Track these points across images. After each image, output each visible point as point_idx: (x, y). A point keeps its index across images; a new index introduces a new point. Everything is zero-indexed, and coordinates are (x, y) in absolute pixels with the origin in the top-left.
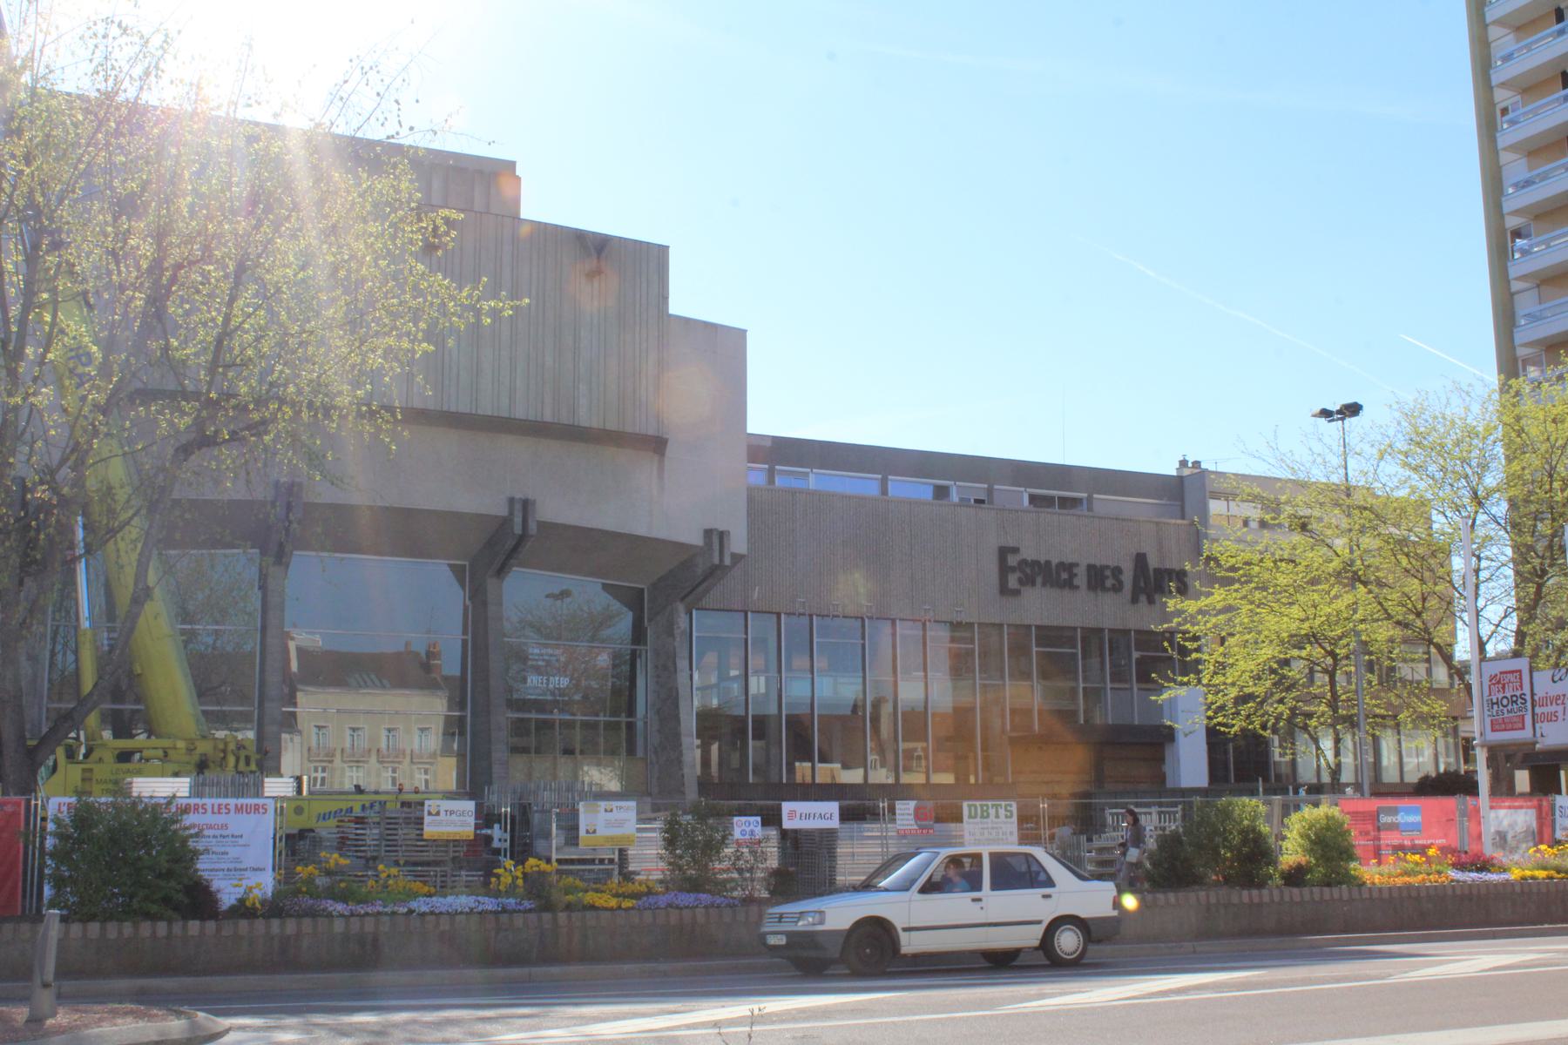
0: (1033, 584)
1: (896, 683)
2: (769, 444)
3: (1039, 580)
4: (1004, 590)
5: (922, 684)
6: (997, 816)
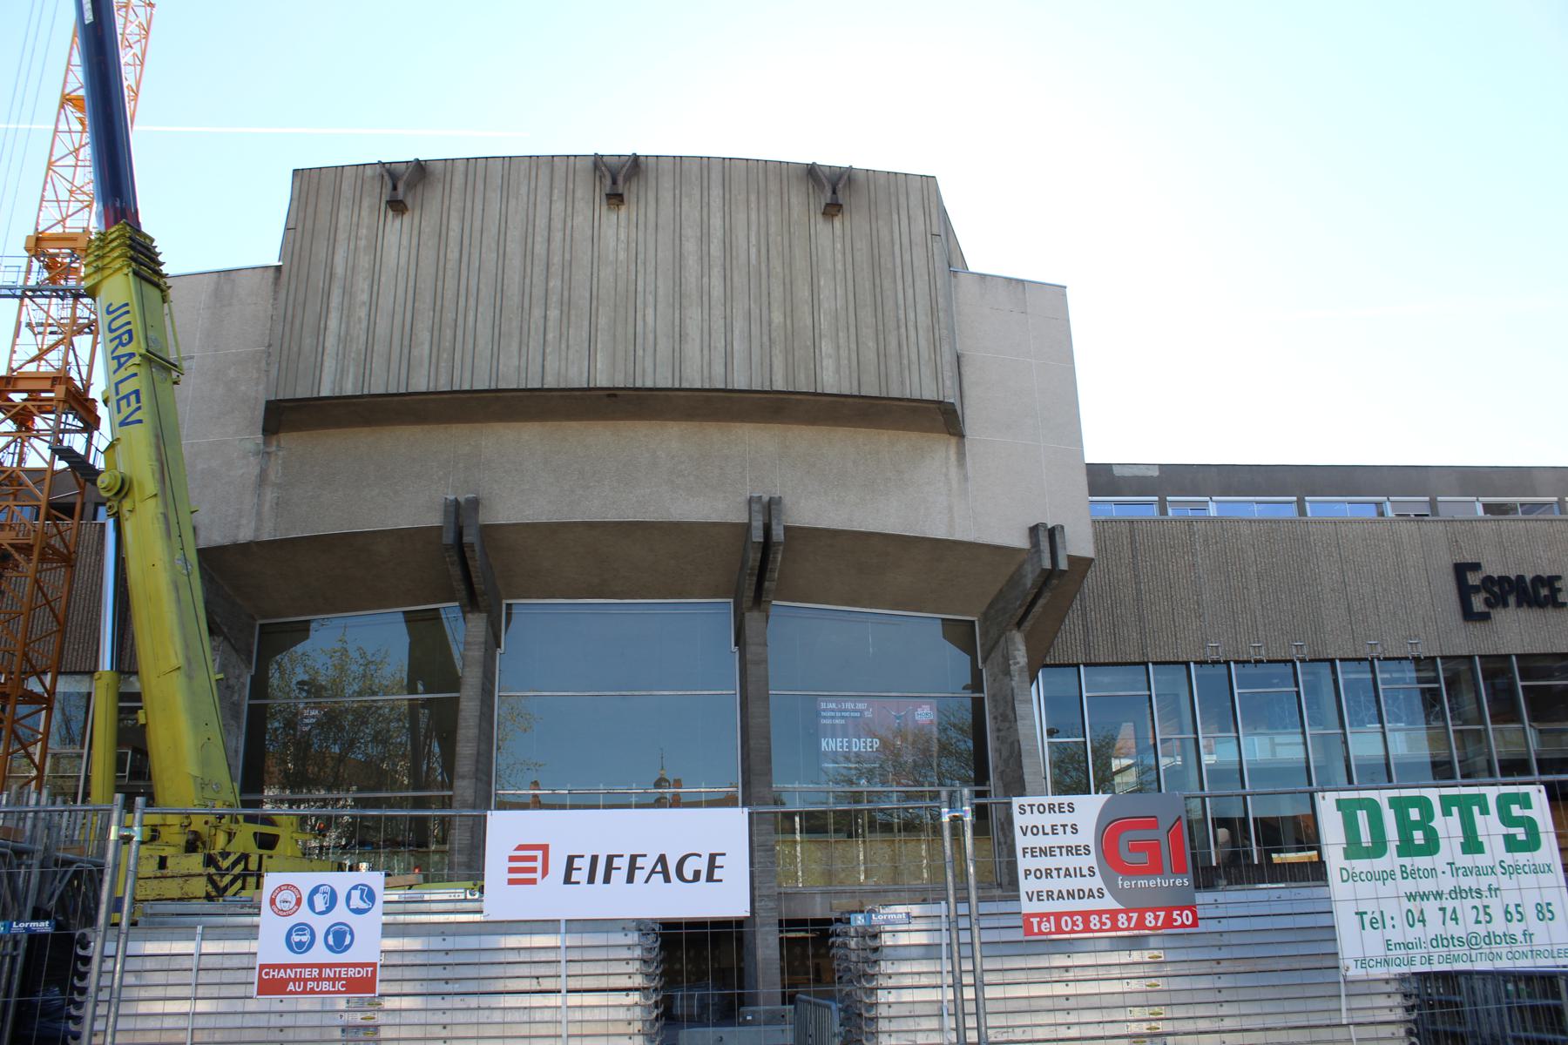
2: (1156, 473)
3: (1512, 600)
4: (1469, 614)
5: (1379, 737)
6: (1472, 844)
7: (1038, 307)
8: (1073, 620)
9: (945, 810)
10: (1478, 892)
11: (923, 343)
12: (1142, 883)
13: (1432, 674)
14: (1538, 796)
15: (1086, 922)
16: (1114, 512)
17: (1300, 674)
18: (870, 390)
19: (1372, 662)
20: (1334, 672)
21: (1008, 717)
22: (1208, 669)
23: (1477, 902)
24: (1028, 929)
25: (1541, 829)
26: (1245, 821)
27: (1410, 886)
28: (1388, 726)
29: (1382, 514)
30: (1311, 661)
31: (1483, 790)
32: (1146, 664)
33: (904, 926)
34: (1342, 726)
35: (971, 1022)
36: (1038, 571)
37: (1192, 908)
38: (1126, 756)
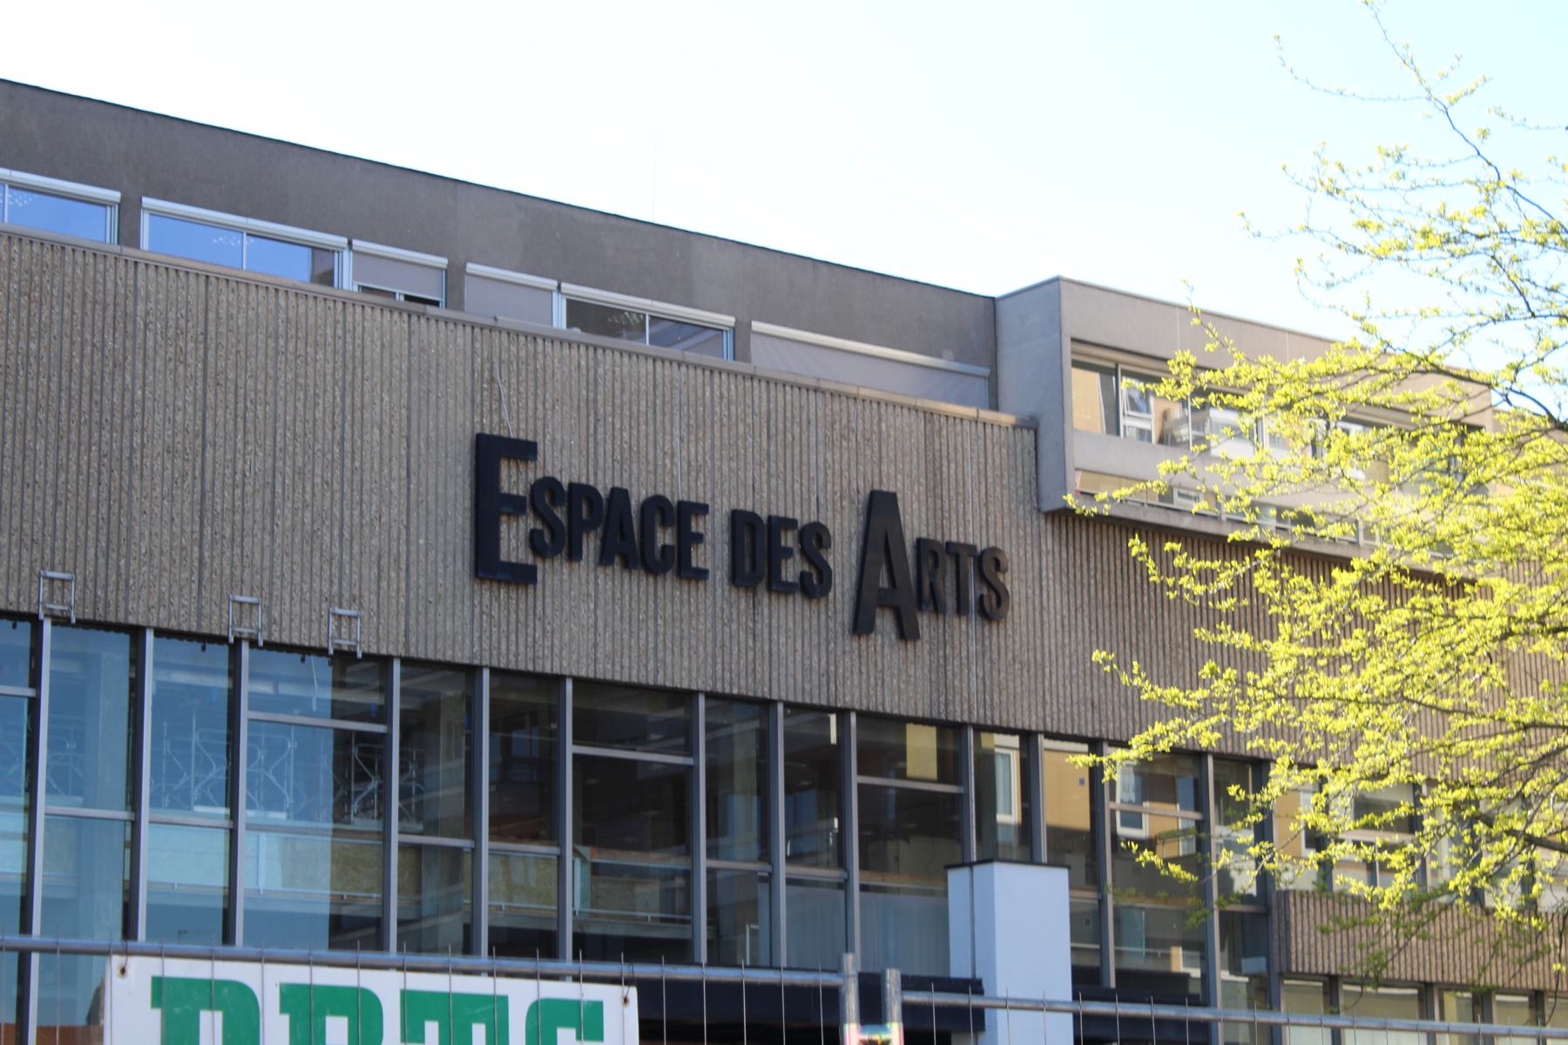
0: (574, 555)
1: (135, 825)
3: (591, 545)
4: (487, 564)
5: (220, 841)
13: (375, 699)
20: (137, 661)
28: (245, 814)
29: (327, 278)
30: (84, 624)
34: (134, 802)
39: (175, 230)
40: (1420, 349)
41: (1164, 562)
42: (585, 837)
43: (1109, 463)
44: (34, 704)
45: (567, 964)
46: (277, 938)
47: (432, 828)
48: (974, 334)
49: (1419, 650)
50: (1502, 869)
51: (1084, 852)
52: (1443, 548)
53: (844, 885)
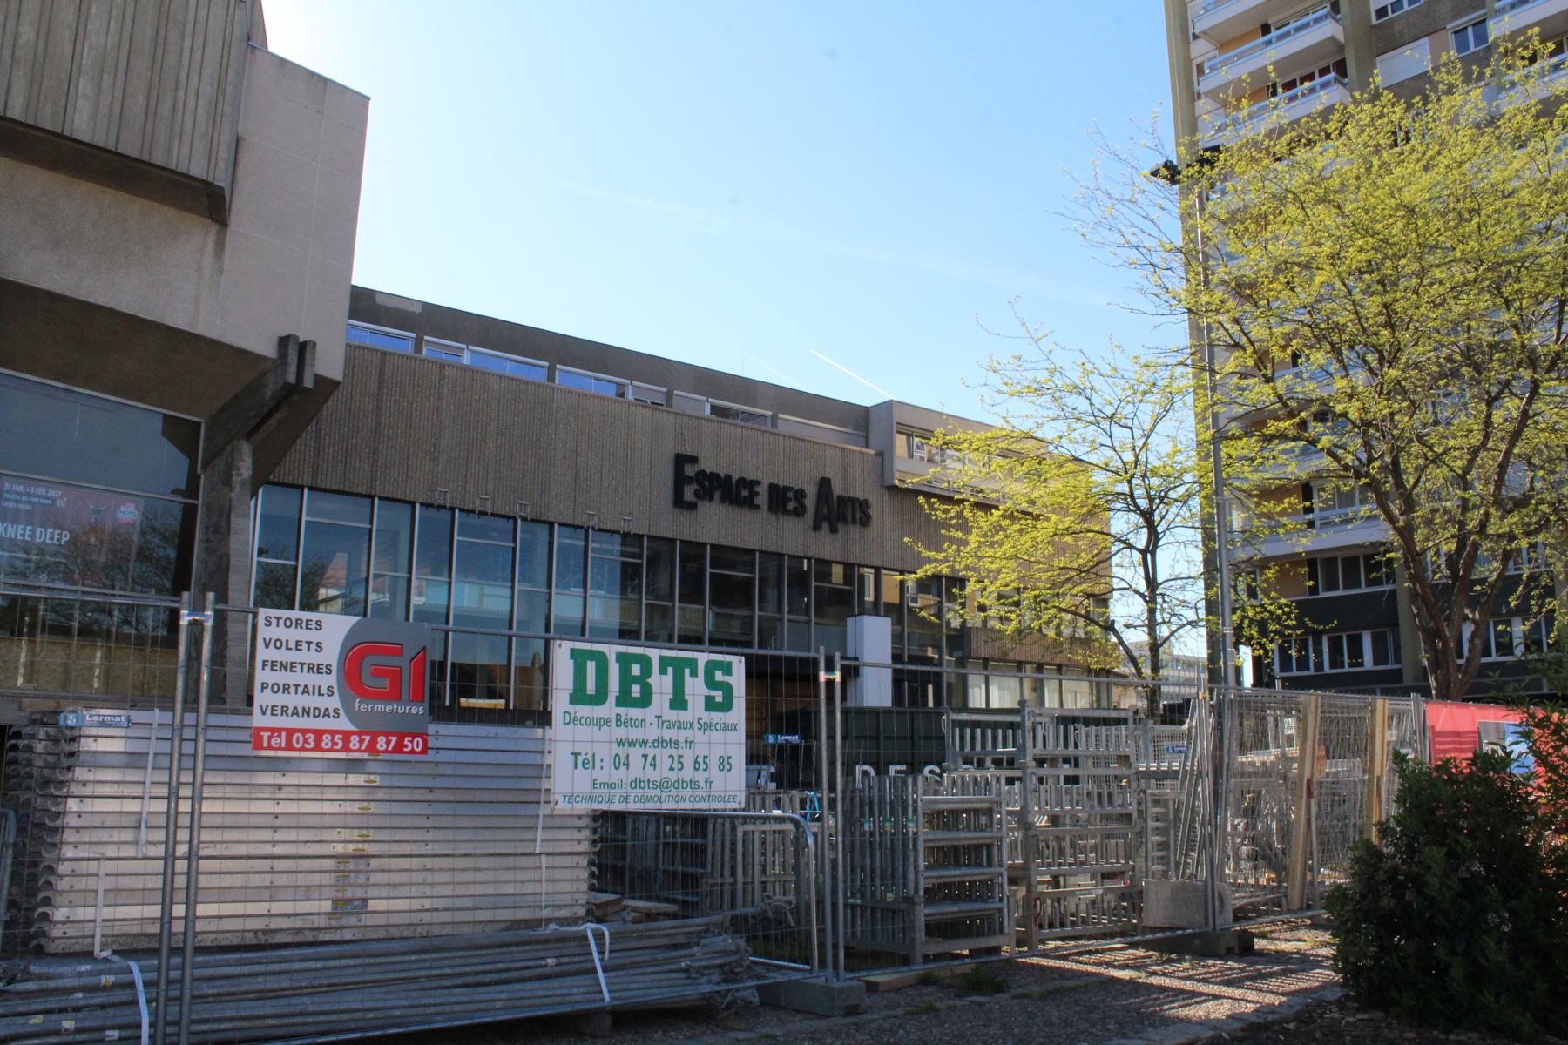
3: (717, 495)
4: (679, 502)
5: (581, 601)
6: (679, 702)
7: (335, 114)
8: (305, 442)
9: (184, 612)
10: (677, 743)
11: (201, 114)
12: (379, 707)
14: (738, 665)
15: (318, 741)
16: (369, 341)
17: (513, 530)
18: (130, 148)
19: (587, 531)
21: (221, 529)
22: (431, 513)
23: (674, 752)
24: (258, 745)
25: (735, 693)
26: (443, 664)
27: (622, 733)
28: (590, 592)
29: (622, 395)
30: (533, 520)
31: (696, 655)
32: (372, 497)
33: (104, 732)
34: (549, 586)
35: (183, 835)
36: (280, 384)
37: (424, 736)
38: (334, 586)
39: (569, 377)
40: (1025, 428)
41: (931, 505)
42: (713, 603)
43: (910, 469)
44: (514, 549)
45: (675, 644)
46: (601, 635)
47: (657, 598)
48: (860, 420)
49: (1023, 539)
50: (1050, 621)
51: (896, 612)
52: (1032, 503)
53: (809, 622)
